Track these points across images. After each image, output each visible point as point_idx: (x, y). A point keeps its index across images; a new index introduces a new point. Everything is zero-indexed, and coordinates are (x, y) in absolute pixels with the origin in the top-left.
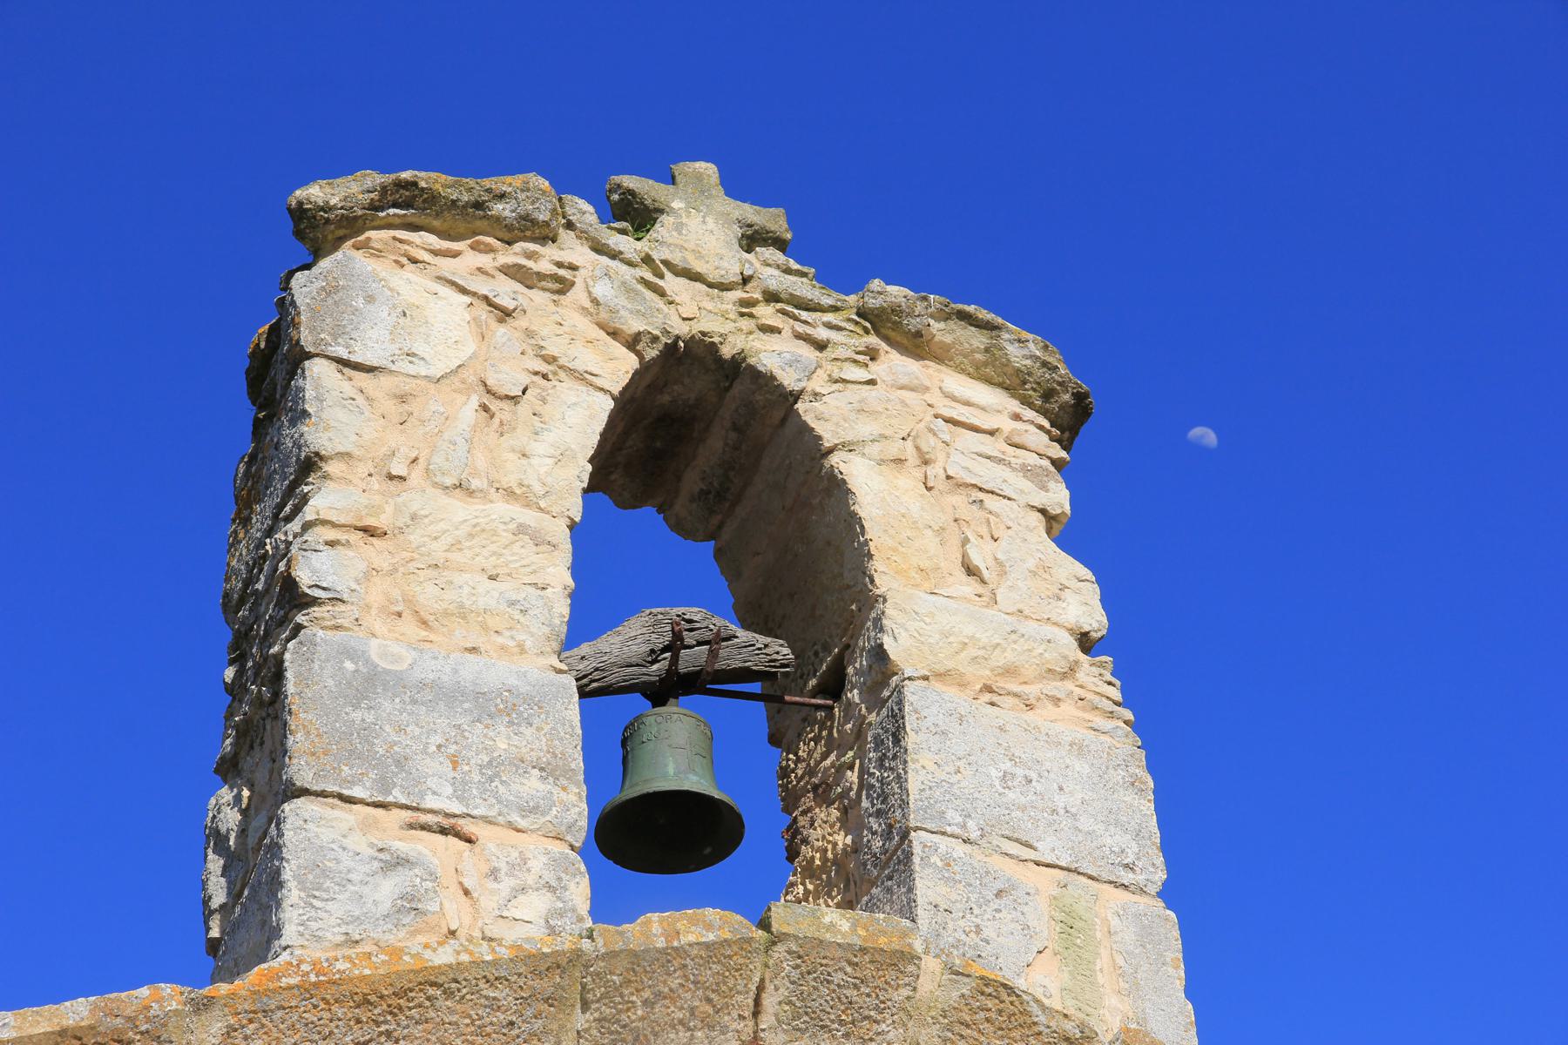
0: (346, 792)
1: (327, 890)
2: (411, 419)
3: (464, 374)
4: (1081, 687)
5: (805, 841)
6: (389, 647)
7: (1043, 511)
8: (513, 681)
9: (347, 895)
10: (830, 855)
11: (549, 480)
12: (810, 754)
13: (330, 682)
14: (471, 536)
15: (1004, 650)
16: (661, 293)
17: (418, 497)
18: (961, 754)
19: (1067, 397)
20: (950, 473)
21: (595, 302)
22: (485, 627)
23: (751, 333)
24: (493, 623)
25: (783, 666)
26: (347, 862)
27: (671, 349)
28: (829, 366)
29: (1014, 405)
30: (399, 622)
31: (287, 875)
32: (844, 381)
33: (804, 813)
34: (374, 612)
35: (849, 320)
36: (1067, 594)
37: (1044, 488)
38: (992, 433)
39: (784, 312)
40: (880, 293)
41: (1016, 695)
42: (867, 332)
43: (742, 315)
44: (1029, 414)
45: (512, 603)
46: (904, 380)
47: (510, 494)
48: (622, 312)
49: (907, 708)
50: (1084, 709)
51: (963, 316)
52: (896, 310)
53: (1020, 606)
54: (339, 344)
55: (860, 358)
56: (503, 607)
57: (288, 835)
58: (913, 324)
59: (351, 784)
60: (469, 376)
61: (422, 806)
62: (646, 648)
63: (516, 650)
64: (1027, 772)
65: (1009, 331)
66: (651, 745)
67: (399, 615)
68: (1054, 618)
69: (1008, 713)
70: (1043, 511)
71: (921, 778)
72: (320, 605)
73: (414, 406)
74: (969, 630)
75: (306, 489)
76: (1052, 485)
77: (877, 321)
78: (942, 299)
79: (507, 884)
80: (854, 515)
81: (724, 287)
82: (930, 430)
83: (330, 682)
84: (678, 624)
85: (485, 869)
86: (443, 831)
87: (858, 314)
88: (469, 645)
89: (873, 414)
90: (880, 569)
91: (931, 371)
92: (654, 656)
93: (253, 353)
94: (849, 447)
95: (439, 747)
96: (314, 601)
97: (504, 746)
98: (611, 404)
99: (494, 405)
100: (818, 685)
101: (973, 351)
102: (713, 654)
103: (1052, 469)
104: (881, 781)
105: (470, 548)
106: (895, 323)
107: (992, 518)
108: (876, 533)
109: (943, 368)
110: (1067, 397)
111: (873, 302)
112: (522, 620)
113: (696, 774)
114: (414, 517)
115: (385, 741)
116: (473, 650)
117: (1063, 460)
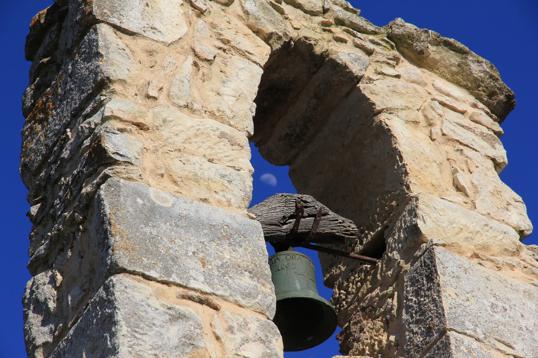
0: (147, 273)
1: (142, 328)
2: (156, 65)
3: (184, 43)
4: (524, 260)
5: (358, 340)
6: (159, 193)
7: (494, 160)
8: (228, 221)
9: (154, 332)
10: (376, 348)
11: (235, 109)
12: (358, 289)
13: (131, 209)
14: (196, 135)
15: (482, 235)
16: (282, 12)
17: (164, 110)
18: (468, 290)
19: (502, 97)
20: (445, 132)
21: (247, 13)
22: (209, 189)
23: (329, 41)
24: (214, 186)
25: (352, 234)
26: (151, 314)
27: (287, 45)
28: (374, 65)
29: (472, 99)
30: (162, 180)
31: (119, 316)
32: (384, 74)
33: (356, 324)
34: (148, 172)
35: (383, 40)
36: (510, 207)
37: (493, 147)
38: (463, 113)
39: (348, 32)
40: (402, 26)
41: (492, 261)
42: (393, 48)
43: (325, 30)
44: (481, 105)
45: (223, 176)
46: (414, 78)
47: (212, 115)
48: (263, 20)
49: (437, 261)
50: (527, 273)
51: (448, 44)
52: (410, 36)
53: (489, 211)
54: (114, 17)
55: (391, 62)
56: (218, 178)
57: (117, 294)
58: (418, 46)
59: (149, 269)
60: (185, 44)
61: (189, 286)
62: (281, 215)
63: (226, 203)
64: (504, 304)
65: (472, 56)
66: (284, 272)
67: (162, 176)
68: (506, 220)
69: (488, 269)
70: (494, 160)
71: (449, 301)
72: (118, 164)
73: (158, 58)
74: (464, 221)
75: (103, 98)
76: (497, 145)
77: (398, 42)
78: (436, 33)
79: (239, 336)
80: (396, 149)
81: (313, 13)
82: (432, 107)
83: (131, 209)
84: (299, 203)
85: (226, 326)
86: (201, 302)
87: (388, 37)
88: (203, 197)
89: (400, 94)
90: (413, 181)
91: (426, 74)
92: (284, 220)
93: (33, 26)
94: (390, 111)
95: (194, 253)
96: (116, 162)
97: (228, 257)
98: (261, 71)
99: (200, 63)
100: (363, 250)
101: (451, 65)
102: (316, 222)
103: (496, 136)
104: (419, 303)
105: (196, 142)
106: (409, 45)
107: (469, 160)
108: (409, 160)
109: (433, 74)
110: (502, 97)
111: (397, 31)
112: (229, 186)
113: (313, 291)
114: (164, 122)
115: (164, 246)
116: (205, 200)
117: (500, 132)
